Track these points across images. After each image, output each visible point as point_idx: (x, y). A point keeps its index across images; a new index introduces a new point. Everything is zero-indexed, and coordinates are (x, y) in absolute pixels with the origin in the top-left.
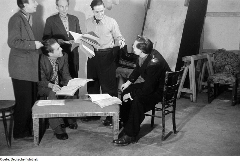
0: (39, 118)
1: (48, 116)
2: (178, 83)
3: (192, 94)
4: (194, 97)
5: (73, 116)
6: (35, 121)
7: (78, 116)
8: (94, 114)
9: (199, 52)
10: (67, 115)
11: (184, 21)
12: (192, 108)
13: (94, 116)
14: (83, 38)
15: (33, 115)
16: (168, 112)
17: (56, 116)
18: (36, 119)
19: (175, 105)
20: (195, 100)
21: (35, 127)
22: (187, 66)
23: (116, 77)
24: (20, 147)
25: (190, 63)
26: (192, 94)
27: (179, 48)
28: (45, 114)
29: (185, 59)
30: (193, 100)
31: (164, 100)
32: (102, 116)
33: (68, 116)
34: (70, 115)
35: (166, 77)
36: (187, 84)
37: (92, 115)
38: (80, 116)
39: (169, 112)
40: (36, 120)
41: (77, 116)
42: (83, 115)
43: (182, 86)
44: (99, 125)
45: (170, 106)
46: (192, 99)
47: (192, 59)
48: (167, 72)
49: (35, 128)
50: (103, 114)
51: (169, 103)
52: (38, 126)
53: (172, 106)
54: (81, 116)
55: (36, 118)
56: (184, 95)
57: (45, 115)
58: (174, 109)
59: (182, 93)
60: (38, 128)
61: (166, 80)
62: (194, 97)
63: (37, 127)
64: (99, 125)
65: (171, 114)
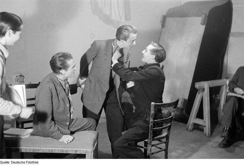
2: (172, 115)
3: (205, 126)
4: (207, 130)
9: (223, 77)
11: (200, 42)
14: (32, 135)
19: (168, 142)
20: (209, 134)
22: (201, 94)
25: (204, 90)
26: (205, 126)
27: (194, 72)
29: (197, 85)
30: (206, 134)
31: (151, 136)
32: (97, 40)
35: (152, 108)
36: (200, 115)
43: (194, 117)
45: (162, 143)
46: (206, 132)
47: (206, 85)
48: (152, 103)
50: (29, 149)
53: (165, 143)
56: (197, 127)
58: (167, 146)
59: (195, 124)
61: (152, 112)
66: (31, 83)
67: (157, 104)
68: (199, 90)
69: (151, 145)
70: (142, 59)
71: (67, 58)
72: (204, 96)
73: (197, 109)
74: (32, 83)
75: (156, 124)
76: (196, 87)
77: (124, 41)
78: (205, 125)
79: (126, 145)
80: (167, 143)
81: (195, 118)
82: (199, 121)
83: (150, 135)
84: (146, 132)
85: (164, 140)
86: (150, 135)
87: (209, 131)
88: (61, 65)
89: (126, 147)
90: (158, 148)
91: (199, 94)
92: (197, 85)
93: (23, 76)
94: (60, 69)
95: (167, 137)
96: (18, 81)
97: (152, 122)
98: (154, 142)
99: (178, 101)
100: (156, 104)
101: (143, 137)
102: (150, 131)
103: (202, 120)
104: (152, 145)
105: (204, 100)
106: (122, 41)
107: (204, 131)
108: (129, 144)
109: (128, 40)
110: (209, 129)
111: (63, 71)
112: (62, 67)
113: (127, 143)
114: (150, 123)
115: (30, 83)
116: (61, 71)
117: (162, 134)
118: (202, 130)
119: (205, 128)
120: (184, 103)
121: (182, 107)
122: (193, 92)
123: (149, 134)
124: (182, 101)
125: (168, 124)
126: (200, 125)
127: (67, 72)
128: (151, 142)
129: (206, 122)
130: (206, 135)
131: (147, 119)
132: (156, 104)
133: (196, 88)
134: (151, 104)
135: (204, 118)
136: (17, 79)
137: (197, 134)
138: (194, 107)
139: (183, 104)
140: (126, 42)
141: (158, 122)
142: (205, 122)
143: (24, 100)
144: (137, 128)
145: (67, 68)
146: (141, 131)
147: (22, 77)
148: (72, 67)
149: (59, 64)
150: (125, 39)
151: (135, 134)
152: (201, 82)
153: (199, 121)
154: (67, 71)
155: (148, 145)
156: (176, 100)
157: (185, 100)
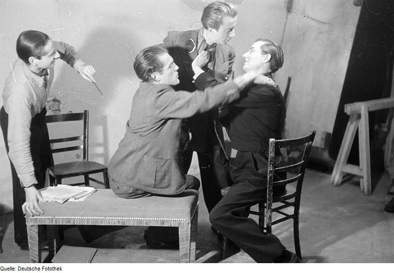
0: (37, 224)
1: (54, 220)
3: (362, 177)
4: (365, 183)
5: (101, 225)
6: (30, 230)
7: (110, 225)
8: (141, 221)
10: (90, 221)
12: (307, 209)
13: (141, 225)
15: (26, 219)
16: (285, 216)
17: (69, 222)
18: (32, 226)
20: (368, 191)
21: (32, 241)
23: (242, 55)
24: (235, 182)
25: (359, 116)
28: (66, 218)
29: (349, 109)
33: (92, 222)
34: (95, 222)
36: (353, 159)
37: (137, 223)
38: (113, 225)
39: (288, 217)
40: (33, 228)
41: (108, 225)
42: (119, 222)
43: (344, 162)
44: (223, 103)
46: (364, 186)
47: (363, 108)
48: (272, 140)
49: (30, 243)
51: (287, 199)
52: (37, 240)
54: (116, 225)
55: (33, 224)
57: (49, 218)
60: (37, 243)
62: (366, 184)
63: (35, 242)
64: (223, 103)
65: (291, 221)
66: (71, 112)
67: (280, 142)
68: (350, 118)
69: (271, 209)
70: (244, 65)
71: (157, 51)
72: (360, 127)
73: (348, 147)
74: (73, 112)
75: (290, 156)
76: (345, 111)
77: (214, 30)
78: (361, 174)
79: (228, 213)
80: (297, 205)
81: (346, 163)
82: (352, 169)
83: (269, 194)
84: (259, 188)
85: (292, 200)
86: (269, 194)
87: (368, 185)
88: (150, 64)
89: (228, 219)
90: (285, 214)
91: (352, 123)
92: (349, 109)
93: (59, 101)
94: (150, 71)
95: (297, 195)
96: (50, 109)
97: (272, 170)
98: (275, 205)
99: (313, 135)
100: (276, 141)
101: (259, 197)
102: (268, 187)
103: (357, 167)
104: (273, 209)
105: (361, 132)
106: (211, 31)
107: (361, 184)
108: (232, 213)
109: (221, 29)
110: (368, 181)
111: (156, 75)
112: (152, 67)
113: (230, 211)
114: (268, 172)
115: (71, 113)
116: (153, 76)
117: (285, 194)
118: (358, 184)
119: (361, 180)
120: (326, 139)
121: (323, 147)
122: (342, 120)
123: (266, 191)
124: (323, 136)
125: (298, 174)
126: (355, 176)
127: (162, 76)
128: (270, 205)
129: (363, 170)
130: (364, 192)
131: (259, 171)
132: (276, 141)
133: (346, 114)
134: (269, 141)
135: (360, 165)
136: (49, 107)
137: (349, 188)
138: (344, 147)
139: (324, 140)
140: (218, 31)
141: (282, 171)
142: (361, 170)
143: (163, 94)
144: (245, 183)
145: (162, 67)
146: (252, 189)
147: (57, 103)
148: (168, 66)
149: (145, 65)
150: (216, 25)
151: (241, 194)
152: (355, 103)
153: (352, 169)
154: (163, 74)
155: (265, 209)
156: (311, 133)
157: (328, 134)
